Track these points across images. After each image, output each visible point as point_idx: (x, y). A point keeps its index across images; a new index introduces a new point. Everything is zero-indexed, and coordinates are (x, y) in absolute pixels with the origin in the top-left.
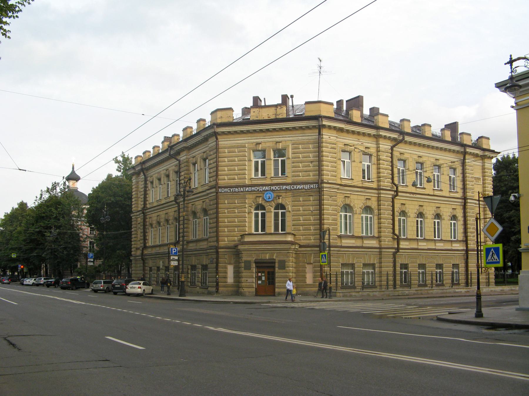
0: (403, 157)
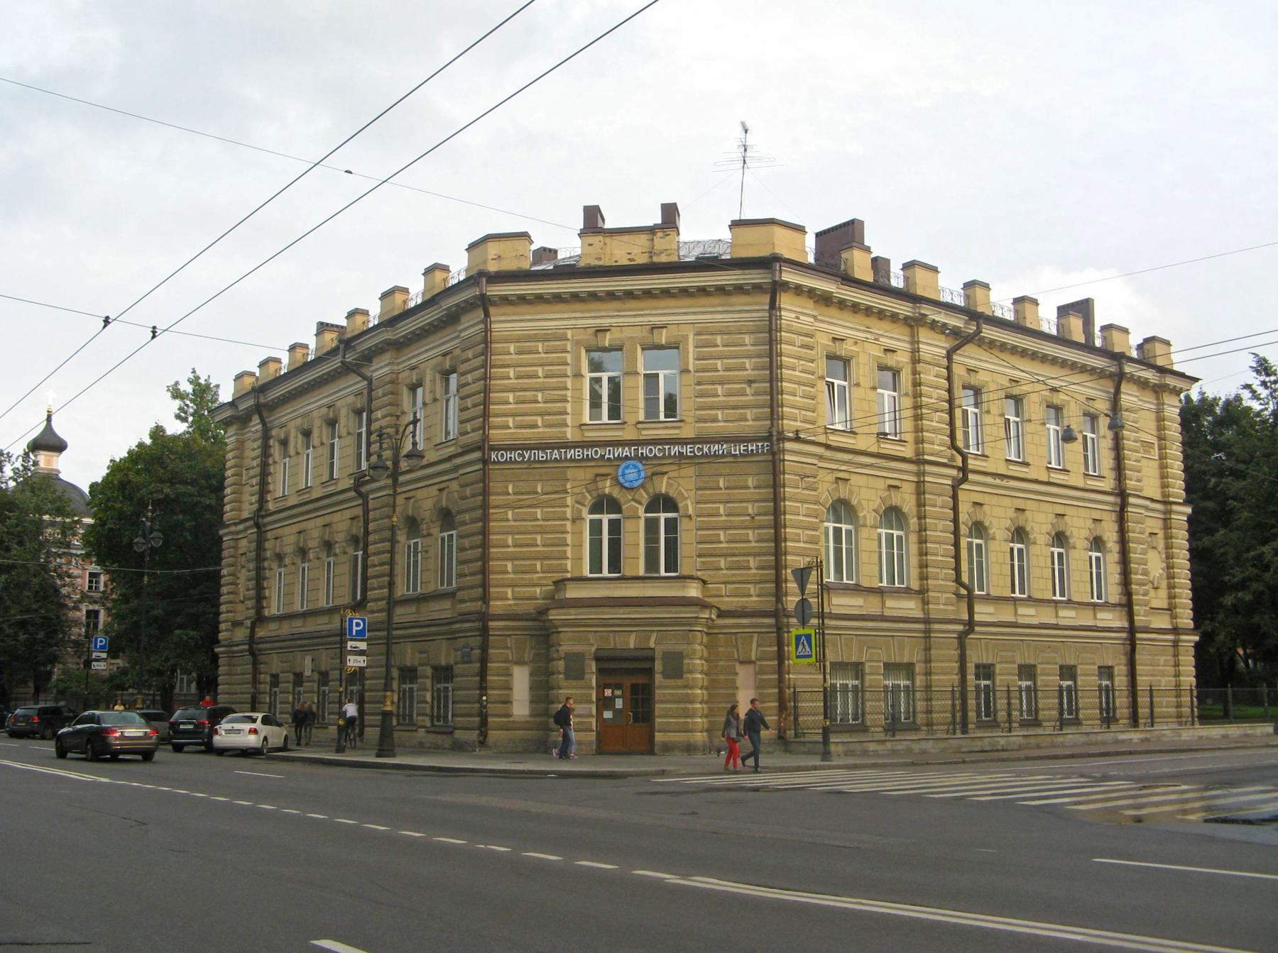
0: (973, 380)
